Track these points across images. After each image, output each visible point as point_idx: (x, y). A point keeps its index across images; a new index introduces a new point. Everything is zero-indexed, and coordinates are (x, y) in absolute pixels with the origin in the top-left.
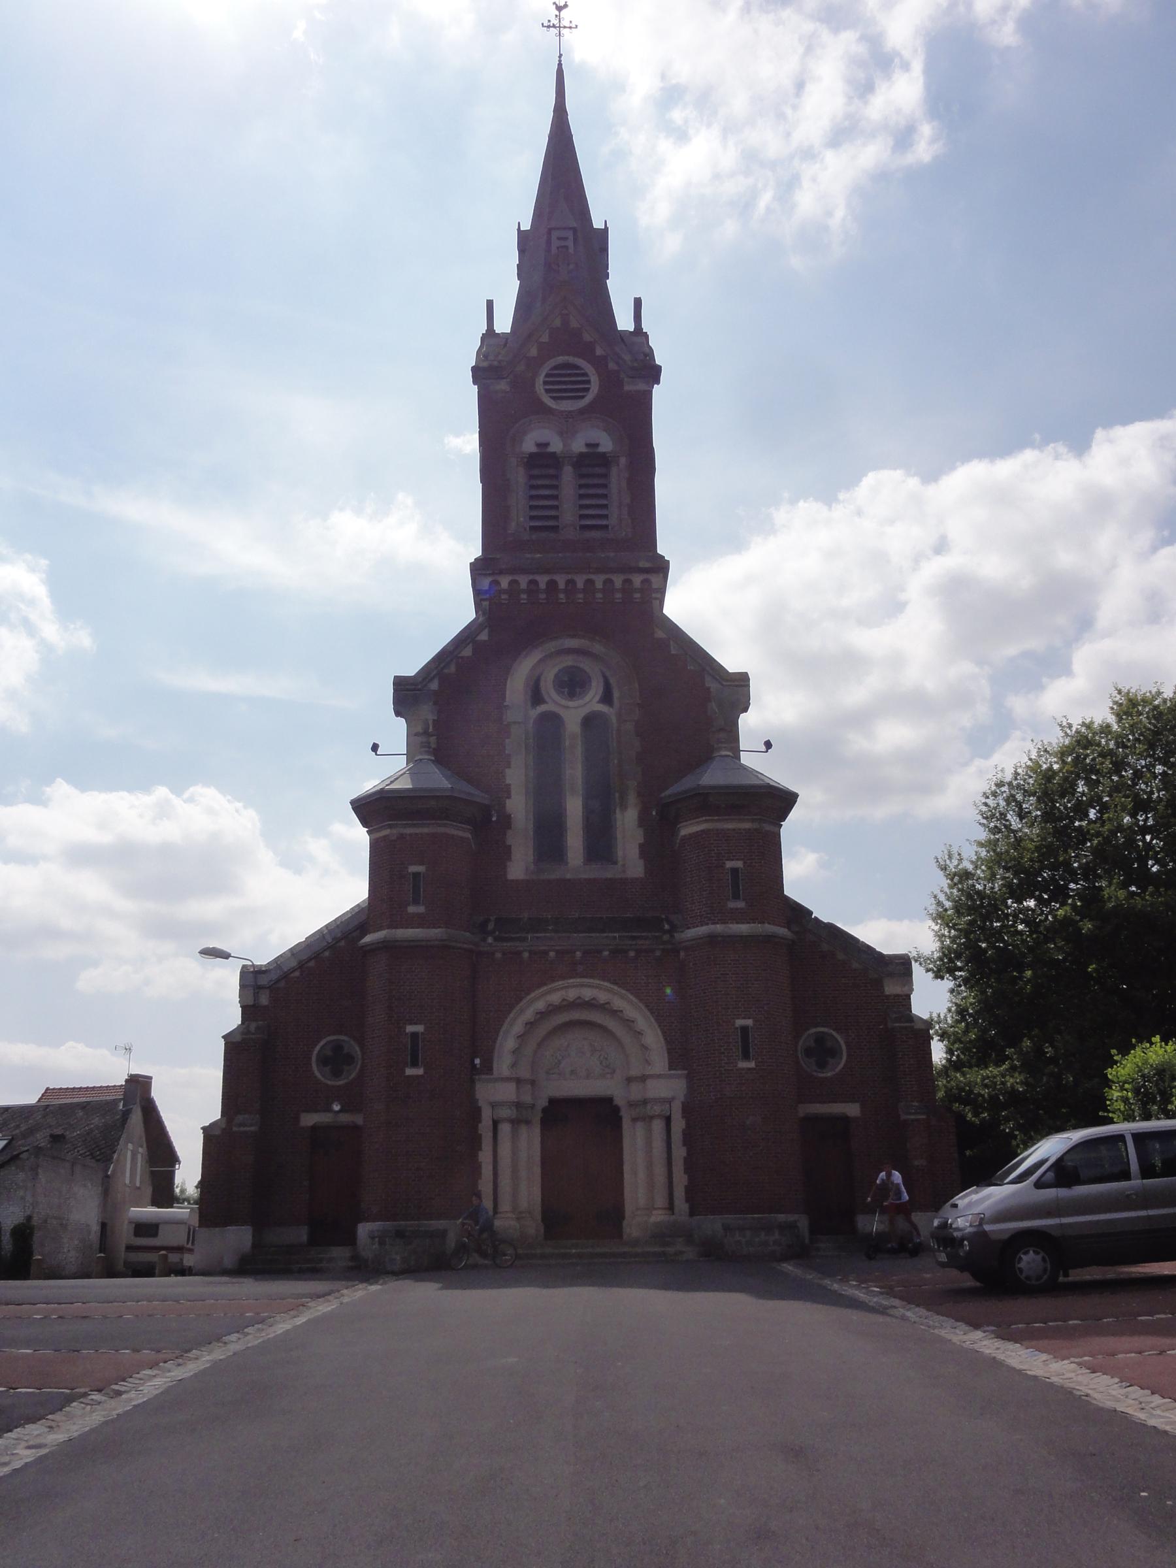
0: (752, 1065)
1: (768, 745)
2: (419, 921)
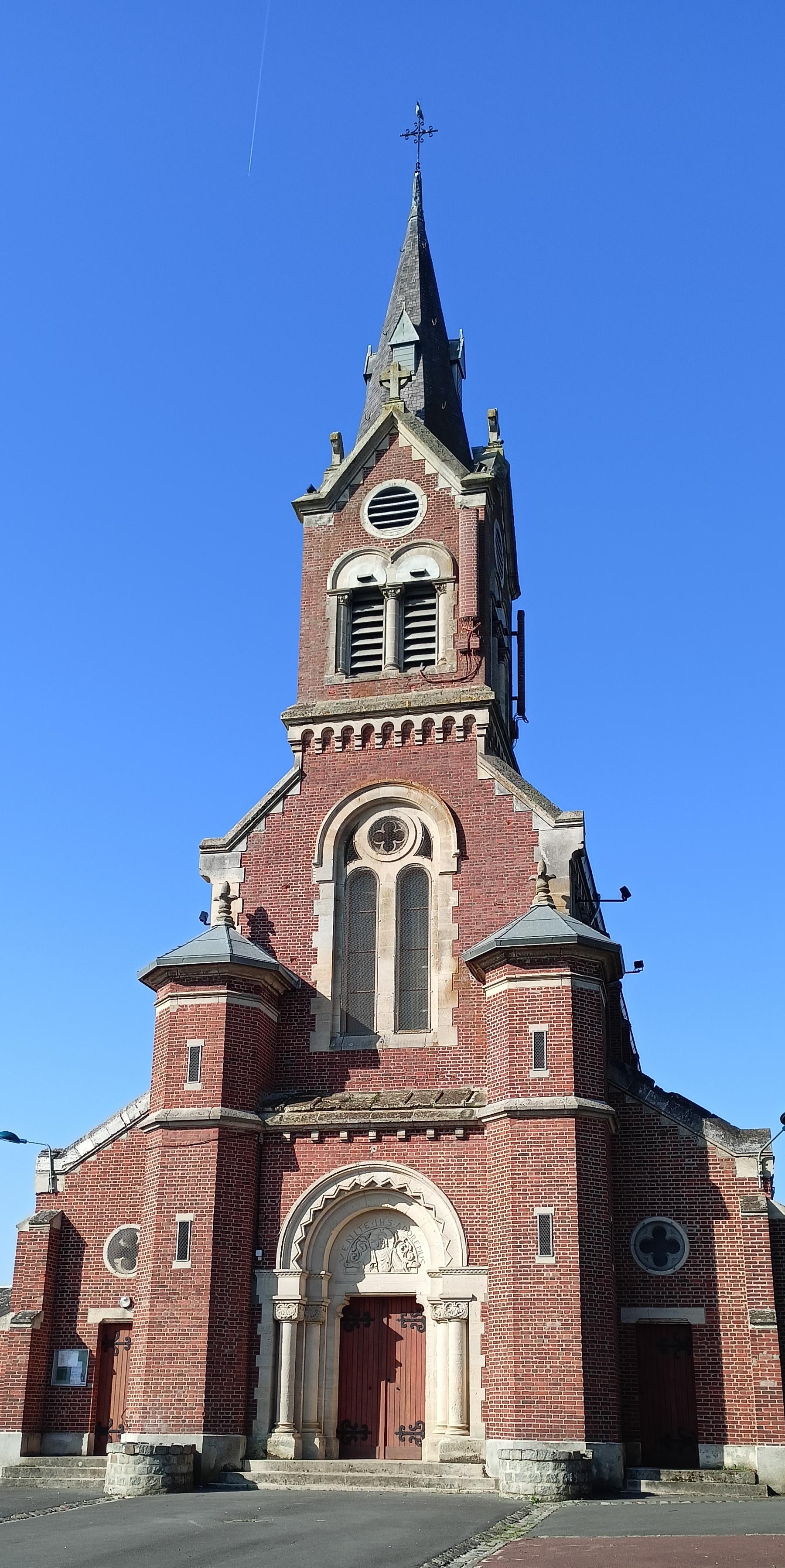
0: (551, 1261)
1: (626, 893)
2: (197, 1099)
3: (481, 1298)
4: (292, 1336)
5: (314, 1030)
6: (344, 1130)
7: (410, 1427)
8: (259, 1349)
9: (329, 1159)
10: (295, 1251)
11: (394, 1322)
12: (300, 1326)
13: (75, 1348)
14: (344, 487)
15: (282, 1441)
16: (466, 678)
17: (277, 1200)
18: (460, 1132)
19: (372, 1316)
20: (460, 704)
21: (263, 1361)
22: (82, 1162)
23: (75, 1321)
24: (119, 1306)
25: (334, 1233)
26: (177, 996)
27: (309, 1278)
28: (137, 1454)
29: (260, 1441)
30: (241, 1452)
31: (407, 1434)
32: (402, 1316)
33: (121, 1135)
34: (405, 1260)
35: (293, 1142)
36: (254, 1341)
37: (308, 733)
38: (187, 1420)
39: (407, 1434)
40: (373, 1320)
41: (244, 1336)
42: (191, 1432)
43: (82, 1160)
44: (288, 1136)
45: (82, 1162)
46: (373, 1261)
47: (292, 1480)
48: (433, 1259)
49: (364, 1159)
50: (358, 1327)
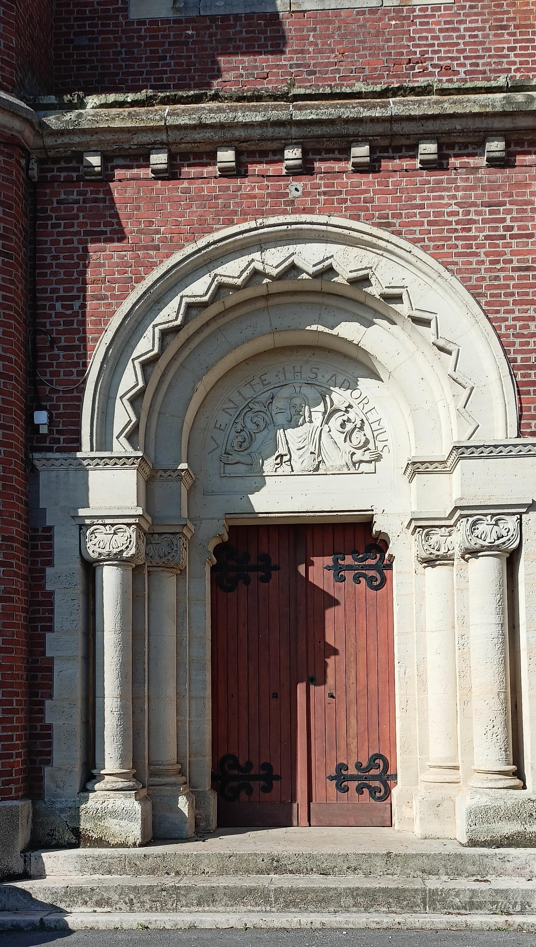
4: (124, 592)
6: (226, 144)
7: (358, 766)
8: (51, 620)
10: (123, 416)
11: (319, 572)
12: (139, 573)
15: (113, 808)
17: (77, 304)
18: (496, 146)
19: (274, 562)
21: (62, 645)
25: (210, 379)
27: (153, 479)
29: (62, 810)
30: (22, 838)
31: (353, 778)
32: (336, 561)
34: (347, 447)
35: (106, 176)
36: (40, 603)
39: (353, 778)
40: (277, 568)
41: (16, 592)
44: (95, 160)
46: (282, 450)
47: (146, 898)
48: (401, 443)
49: (273, 213)
50: (247, 582)
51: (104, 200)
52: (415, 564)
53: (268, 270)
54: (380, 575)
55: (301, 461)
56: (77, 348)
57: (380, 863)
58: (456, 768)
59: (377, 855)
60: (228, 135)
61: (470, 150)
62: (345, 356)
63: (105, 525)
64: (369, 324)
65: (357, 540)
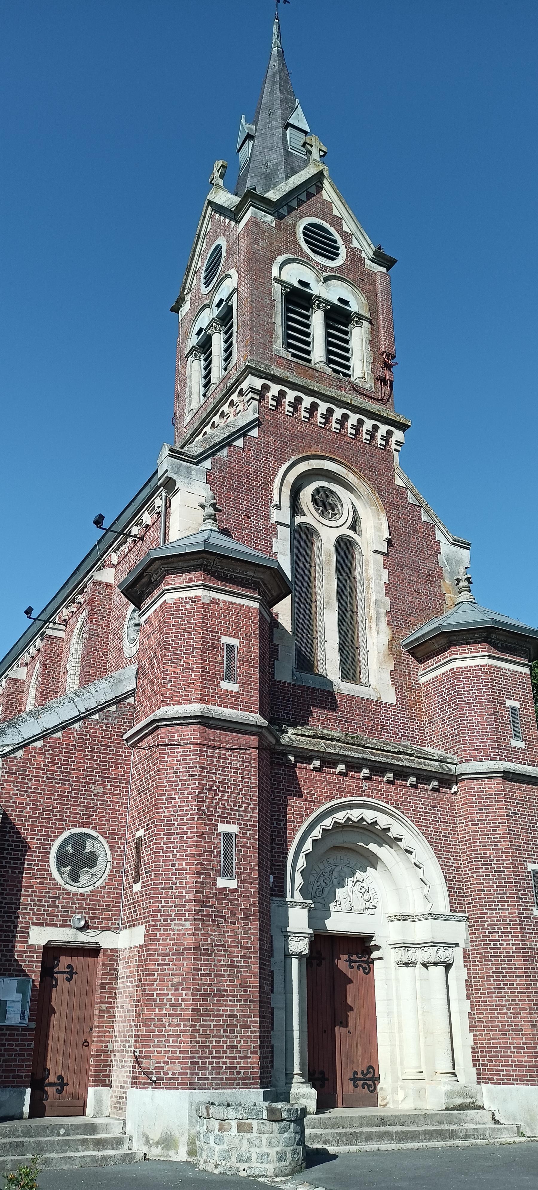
2: (235, 701)
3: (462, 945)
5: (277, 659)
7: (362, 1072)
9: (327, 789)
11: (342, 963)
13: (10, 975)
14: (284, 203)
16: (381, 400)
17: (282, 823)
20: (386, 418)
22: (24, 746)
23: (11, 941)
24: (70, 926)
26: (211, 587)
28: (284, 1120)
31: (360, 1079)
32: (349, 957)
33: (72, 723)
37: (266, 388)
38: (242, 1071)
39: (360, 1079)
40: (324, 959)
42: (246, 1086)
43: (25, 745)
45: (24, 746)
46: (337, 899)
47: (344, 1139)
51: (293, 776)
52: (393, 964)
53: (353, 819)
54: (368, 968)
55: (345, 906)
56: (282, 845)
57: (422, 1119)
58: (422, 1072)
59: (421, 1115)
60: (346, 759)
61: (425, 782)
62: (358, 853)
63: (295, 937)
64: (380, 846)
65: (361, 946)
